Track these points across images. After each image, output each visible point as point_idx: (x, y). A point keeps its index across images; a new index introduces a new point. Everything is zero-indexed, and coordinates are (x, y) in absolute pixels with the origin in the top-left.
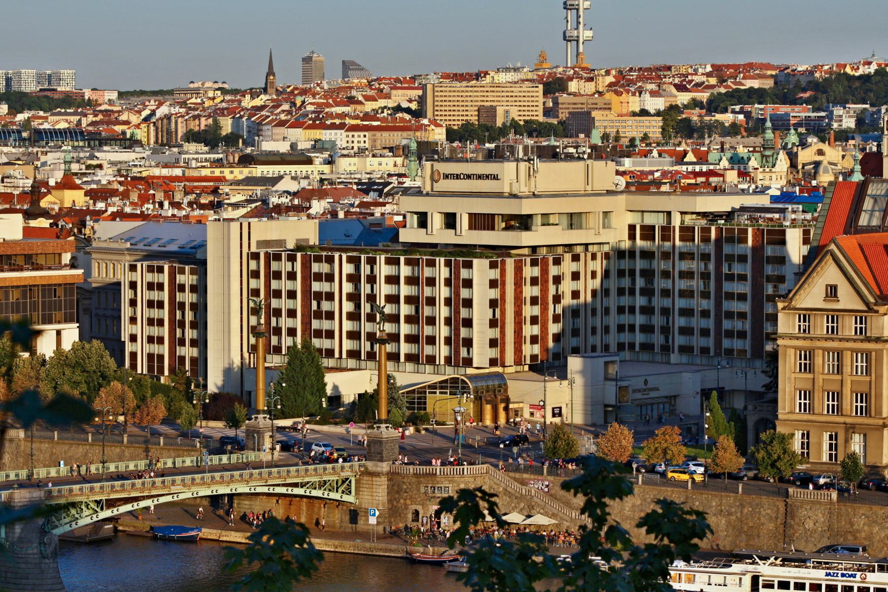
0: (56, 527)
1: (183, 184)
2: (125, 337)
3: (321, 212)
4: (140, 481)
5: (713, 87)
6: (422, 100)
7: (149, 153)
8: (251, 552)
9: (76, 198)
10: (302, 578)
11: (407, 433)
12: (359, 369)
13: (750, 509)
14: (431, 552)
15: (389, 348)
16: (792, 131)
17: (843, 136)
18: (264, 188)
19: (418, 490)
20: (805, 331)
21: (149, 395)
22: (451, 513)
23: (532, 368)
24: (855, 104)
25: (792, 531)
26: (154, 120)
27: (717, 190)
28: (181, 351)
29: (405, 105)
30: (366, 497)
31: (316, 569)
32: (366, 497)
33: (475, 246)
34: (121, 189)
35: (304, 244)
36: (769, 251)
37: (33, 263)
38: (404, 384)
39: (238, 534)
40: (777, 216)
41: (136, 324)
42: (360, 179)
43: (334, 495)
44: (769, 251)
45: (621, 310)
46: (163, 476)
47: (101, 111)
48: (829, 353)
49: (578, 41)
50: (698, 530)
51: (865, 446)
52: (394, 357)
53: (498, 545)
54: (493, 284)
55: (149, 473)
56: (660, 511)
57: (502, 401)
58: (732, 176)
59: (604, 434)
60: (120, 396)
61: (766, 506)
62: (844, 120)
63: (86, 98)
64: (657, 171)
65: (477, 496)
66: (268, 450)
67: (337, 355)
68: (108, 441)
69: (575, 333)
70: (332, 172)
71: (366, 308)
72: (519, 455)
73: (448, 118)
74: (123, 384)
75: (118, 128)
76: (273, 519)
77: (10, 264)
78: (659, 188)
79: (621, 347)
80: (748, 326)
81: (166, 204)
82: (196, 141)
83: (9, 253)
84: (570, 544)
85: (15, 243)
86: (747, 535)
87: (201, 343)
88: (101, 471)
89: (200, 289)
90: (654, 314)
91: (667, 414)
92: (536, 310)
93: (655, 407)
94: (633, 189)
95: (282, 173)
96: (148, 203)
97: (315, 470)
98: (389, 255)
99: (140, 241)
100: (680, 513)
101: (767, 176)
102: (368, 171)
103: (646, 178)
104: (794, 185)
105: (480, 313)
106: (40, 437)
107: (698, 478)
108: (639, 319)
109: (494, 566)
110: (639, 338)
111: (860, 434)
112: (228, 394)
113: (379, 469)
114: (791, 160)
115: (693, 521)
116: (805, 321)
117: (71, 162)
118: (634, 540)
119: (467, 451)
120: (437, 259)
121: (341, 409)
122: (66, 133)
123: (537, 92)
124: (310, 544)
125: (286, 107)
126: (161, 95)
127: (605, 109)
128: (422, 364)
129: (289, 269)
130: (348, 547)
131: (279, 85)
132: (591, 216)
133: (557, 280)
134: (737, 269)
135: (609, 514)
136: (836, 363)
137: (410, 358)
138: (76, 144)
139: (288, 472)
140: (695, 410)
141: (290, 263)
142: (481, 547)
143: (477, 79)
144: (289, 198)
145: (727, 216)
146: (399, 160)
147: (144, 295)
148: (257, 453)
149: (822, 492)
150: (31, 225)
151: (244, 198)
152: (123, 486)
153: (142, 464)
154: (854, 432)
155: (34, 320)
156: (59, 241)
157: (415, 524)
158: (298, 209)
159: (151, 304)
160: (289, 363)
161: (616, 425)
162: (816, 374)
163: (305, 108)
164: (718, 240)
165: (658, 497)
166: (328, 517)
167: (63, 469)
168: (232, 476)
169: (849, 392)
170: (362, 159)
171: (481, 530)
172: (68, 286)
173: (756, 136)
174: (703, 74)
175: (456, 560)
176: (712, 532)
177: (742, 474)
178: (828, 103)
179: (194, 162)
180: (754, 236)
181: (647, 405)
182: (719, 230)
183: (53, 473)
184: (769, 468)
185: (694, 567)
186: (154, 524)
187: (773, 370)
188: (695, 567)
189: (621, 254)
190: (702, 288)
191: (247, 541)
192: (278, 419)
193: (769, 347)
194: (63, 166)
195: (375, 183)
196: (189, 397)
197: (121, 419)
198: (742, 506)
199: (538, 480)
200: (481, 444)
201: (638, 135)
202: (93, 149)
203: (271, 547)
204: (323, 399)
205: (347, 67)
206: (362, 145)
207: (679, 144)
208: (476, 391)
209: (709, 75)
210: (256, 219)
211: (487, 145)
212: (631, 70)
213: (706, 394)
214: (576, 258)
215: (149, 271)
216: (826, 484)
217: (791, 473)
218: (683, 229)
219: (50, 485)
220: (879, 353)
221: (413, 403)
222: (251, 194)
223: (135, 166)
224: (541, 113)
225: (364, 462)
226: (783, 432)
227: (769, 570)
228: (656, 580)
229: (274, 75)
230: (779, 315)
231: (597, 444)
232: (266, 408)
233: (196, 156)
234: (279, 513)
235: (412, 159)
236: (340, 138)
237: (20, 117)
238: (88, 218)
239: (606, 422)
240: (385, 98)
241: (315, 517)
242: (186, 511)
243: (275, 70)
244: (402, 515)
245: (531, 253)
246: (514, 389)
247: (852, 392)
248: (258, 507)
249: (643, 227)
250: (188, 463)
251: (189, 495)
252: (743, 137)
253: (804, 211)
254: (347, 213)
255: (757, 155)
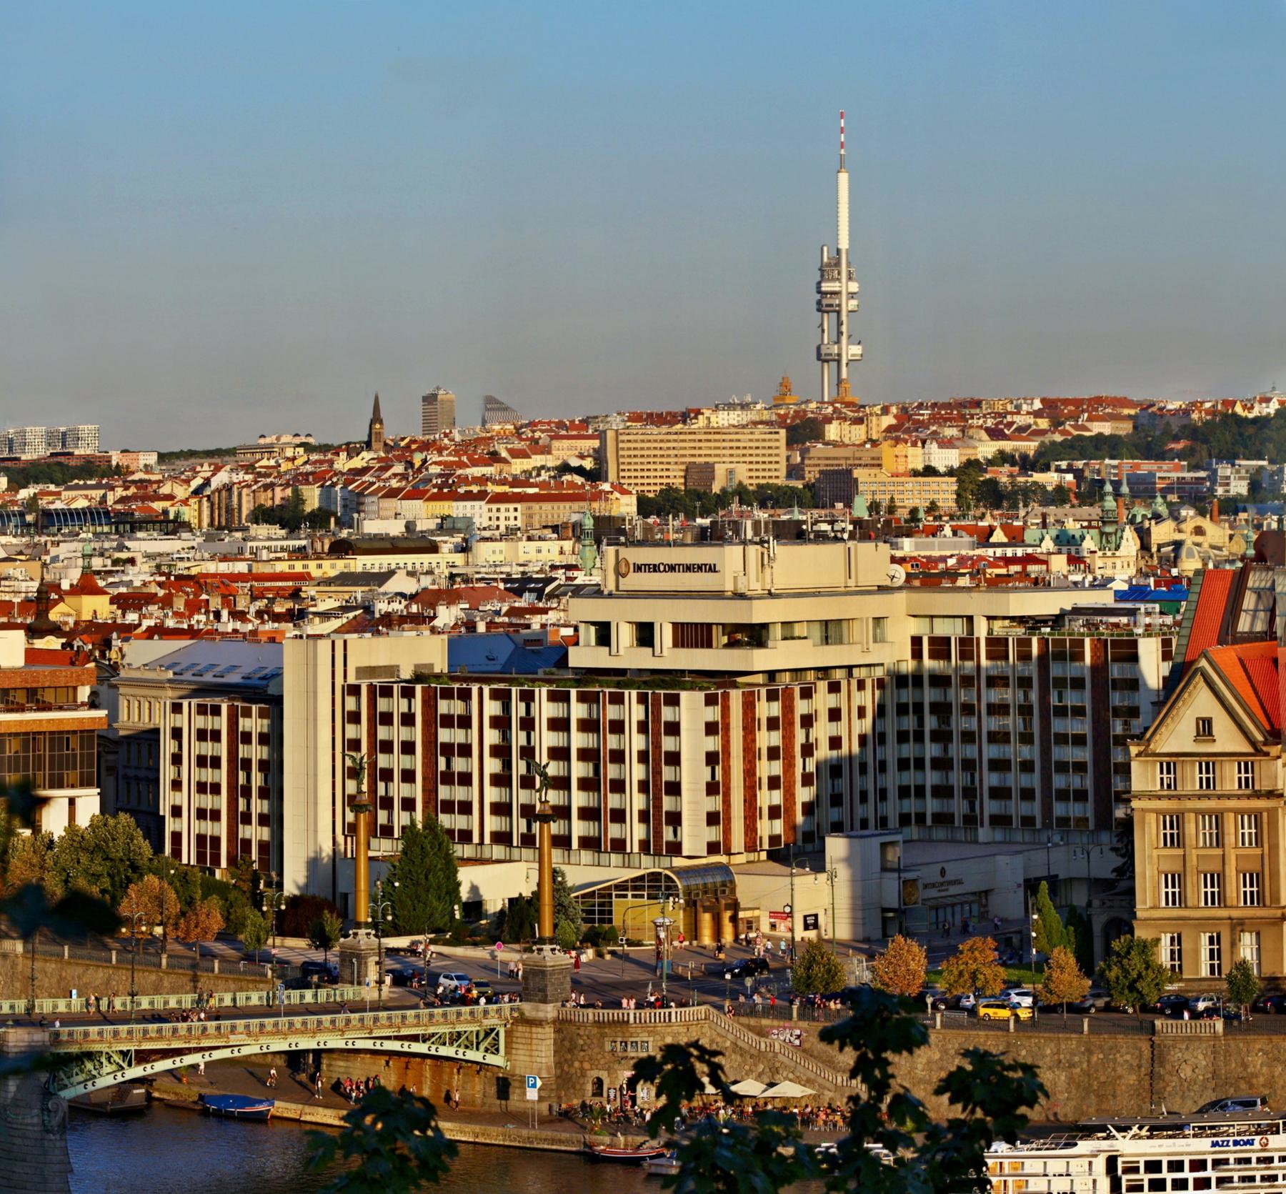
0: (65, 1087)
1: (249, 585)
2: (165, 810)
3: (452, 624)
4: (185, 1025)
5: (1043, 432)
6: (599, 455)
7: (200, 540)
8: (348, 1140)
9: (98, 607)
10: (424, 1183)
11: (584, 958)
12: (510, 861)
13: (1101, 1056)
14: (622, 1144)
15: (555, 828)
16: (1159, 500)
17: (1231, 507)
18: (367, 588)
19: (602, 1046)
20: (1169, 786)
21: (198, 895)
22: (652, 1083)
23: (772, 856)
24: (1248, 459)
25: (1162, 1084)
26: (207, 492)
27: (1039, 584)
28: (245, 832)
29: (575, 462)
30: (522, 1058)
31: (446, 1169)
32: (522, 1058)
33: (683, 672)
34: (161, 593)
35: (426, 671)
36: (1115, 671)
37: (38, 701)
38: (578, 883)
39: (329, 1112)
40: (1124, 620)
41: (180, 790)
42: (509, 574)
43: (473, 1055)
44: (1115, 671)
45: (903, 764)
46: (217, 1018)
47: (134, 482)
48: (1204, 817)
49: (839, 362)
50: (1026, 1093)
51: (1259, 950)
52: (562, 842)
53: (725, 1131)
54: (711, 729)
55: (198, 1014)
56: (969, 1068)
57: (728, 907)
58: (1059, 564)
59: (882, 954)
60: (156, 897)
61: (1123, 1050)
62: (1233, 483)
63: (114, 463)
64: (951, 556)
65: (691, 1055)
66: (373, 984)
67: (476, 839)
68: (140, 964)
69: (836, 800)
70: (467, 564)
71: (519, 767)
72: (755, 990)
73: (639, 481)
74: (161, 878)
75: (158, 506)
76: (380, 1090)
77: (7, 702)
78: (954, 582)
79: (905, 820)
80: (1089, 783)
81: (225, 614)
82: (267, 522)
83: (6, 686)
84: (835, 1125)
85: (14, 672)
86: (1098, 1096)
87: (274, 820)
88: (128, 1008)
89: (273, 739)
90: (952, 769)
91: (975, 920)
92: (777, 768)
93: (958, 908)
94: (917, 583)
95: (393, 567)
96: (199, 613)
97: (445, 1015)
98: (553, 688)
99: (187, 669)
100: (999, 1068)
101: (1109, 562)
102: (521, 562)
103: (936, 568)
104: (1147, 576)
105: (693, 774)
106: (45, 953)
107: (1024, 1014)
108: (931, 778)
109: (720, 1164)
110: (931, 805)
111: (1251, 932)
112: (314, 897)
113: (541, 1015)
114: (1141, 539)
115: (1019, 1080)
116: (1169, 772)
117: (91, 556)
118: (931, 1115)
119: (675, 984)
120: (626, 692)
121: (483, 922)
122: (85, 514)
123: (777, 440)
124: (437, 1130)
125: (399, 468)
126: (217, 455)
127: (873, 465)
128: (606, 852)
129: (404, 709)
130: (495, 1135)
131: (389, 436)
132: (856, 624)
133: (808, 721)
134: (1071, 698)
135: (893, 1076)
136: (1214, 831)
137: (587, 843)
138: (99, 529)
139: (404, 1017)
140: (1016, 912)
141: (405, 701)
142: (699, 1135)
143: (684, 422)
144: (404, 603)
145: (1054, 621)
146: (568, 545)
147: (193, 748)
148: (356, 987)
149: (1203, 1022)
150: (36, 646)
151: (337, 604)
152: (159, 1031)
153: (188, 1000)
154: (1242, 931)
155: (38, 782)
156: (74, 669)
157: (597, 1099)
158: (418, 620)
159: (202, 761)
160: (404, 852)
161: (900, 939)
162: (1188, 849)
163: (427, 469)
164: (1043, 657)
165: (966, 1046)
166: (464, 1088)
167: (76, 1002)
168: (320, 1022)
169: (1234, 873)
170: (510, 544)
171: (699, 1108)
172: (86, 735)
173: (1091, 505)
174: (1028, 413)
175: (661, 1156)
176: (1047, 1095)
177: (1088, 1004)
178: (1210, 457)
179: (265, 552)
180: (1093, 650)
181: (945, 906)
182: (1044, 642)
183: (62, 1006)
184: (1126, 992)
185: (1022, 1150)
186: (206, 1091)
187: (1126, 846)
188: (1023, 1150)
189: (901, 680)
190: (1021, 728)
191: (342, 1123)
192: (387, 936)
193: (1119, 813)
194: (80, 562)
195: (531, 580)
196: (257, 901)
197: (158, 930)
198: (1089, 1052)
199: (785, 1028)
200: (696, 974)
201: (922, 505)
202: (122, 536)
203: (378, 1133)
204: (456, 907)
205: (493, 405)
206: (512, 523)
207: (982, 517)
208: (688, 893)
209: (1037, 414)
210: (355, 636)
211: (699, 521)
212: (920, 406)
213: (1031, 886)
214: (834, 688)
215: (199, 713)
216: (1207, 1009)
217: (1157, 998)
218: (991, 641)
219: (57, 1024)
220: (1273, 813)
221: (593, 912)
222: (347, 597)
223: (181, 559)
224: (783, 472)
225: (518, 1003)
226: (1144, 937)
227: (1133, 1147)
228: (966, 1174)
229: (381, 422)
230: (1133, 764)
231: (873, 970)
232: (370, 920)
233: (267, 544)
234: (390, 1080)
235: (587, 542)
236: (479, 513)
237: (24, 494)
238: (115, 635)
239: (885, 935)
240: (542, 453)
241: (444, 1088)
242: (251, 1074)
243: (382, 415)
244: (578, 1087)
245: (766, 681)
246: (747, 889)
247: (1238, 872)
248: (358, 1072)
249: (933, 640)
250: (255, 1000)
251: (254, 1049)
252: (1073, 506)
253: (1162, 613)
254: (490, 625)
255: (1094, 532)
